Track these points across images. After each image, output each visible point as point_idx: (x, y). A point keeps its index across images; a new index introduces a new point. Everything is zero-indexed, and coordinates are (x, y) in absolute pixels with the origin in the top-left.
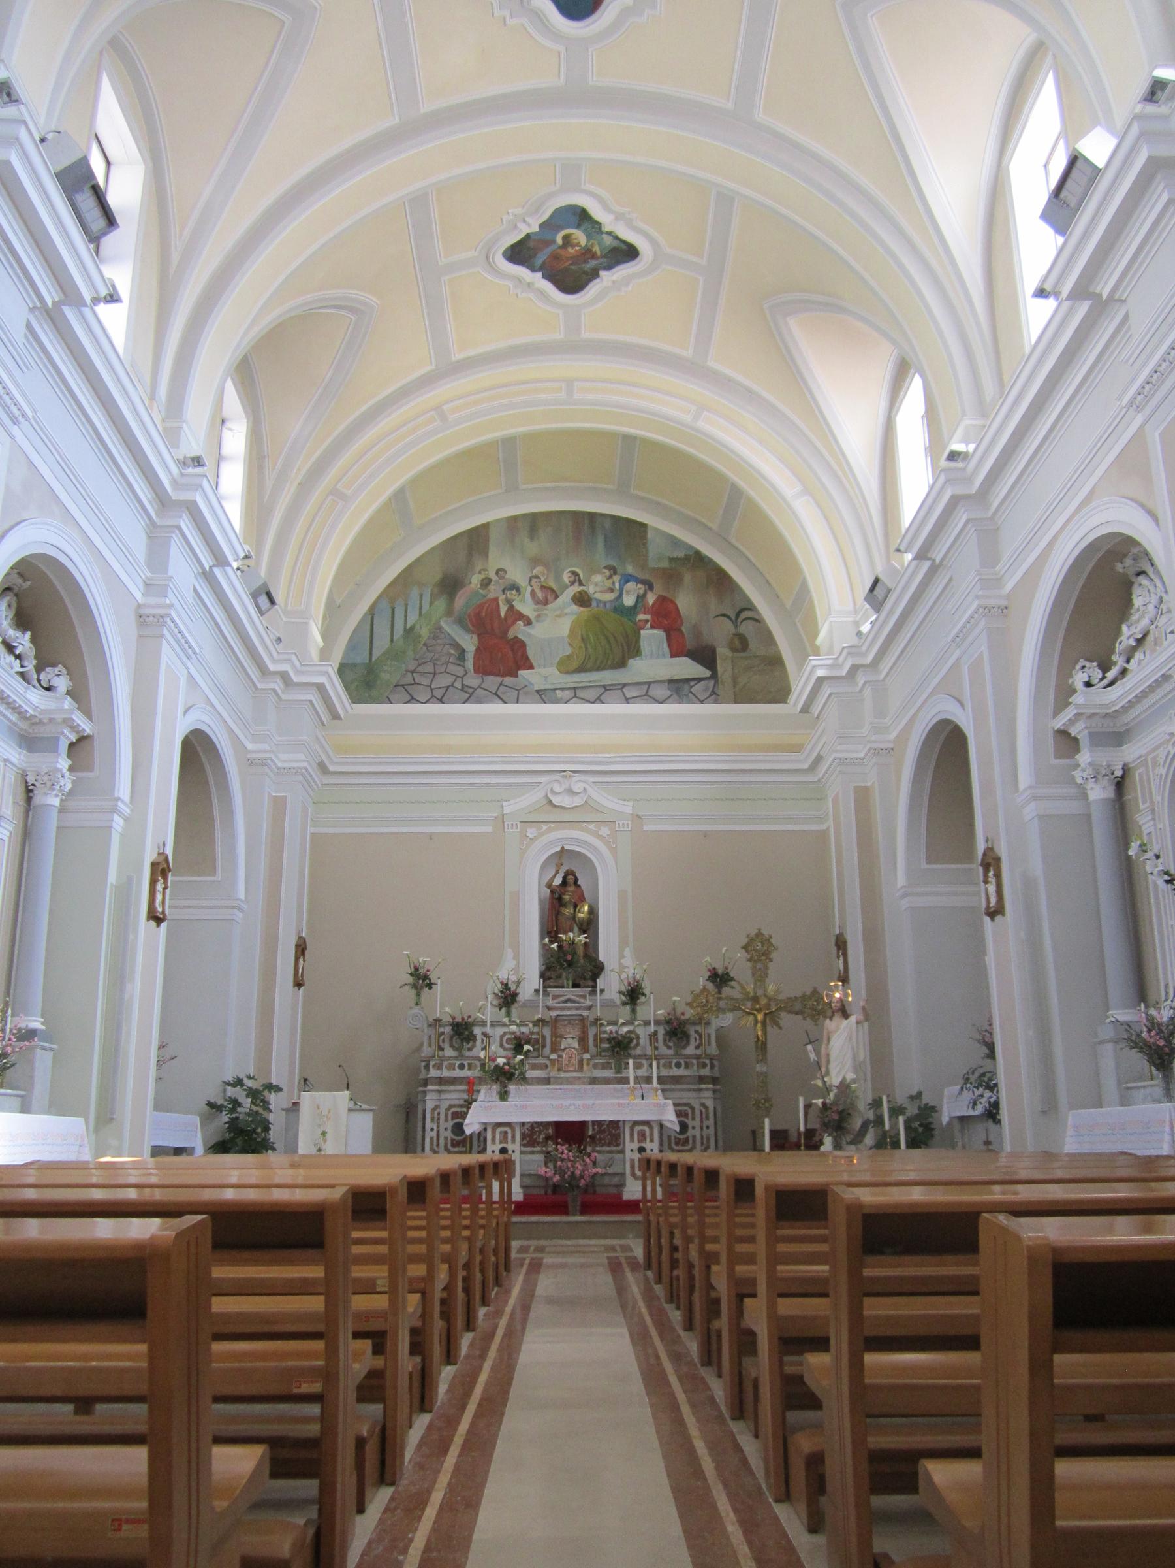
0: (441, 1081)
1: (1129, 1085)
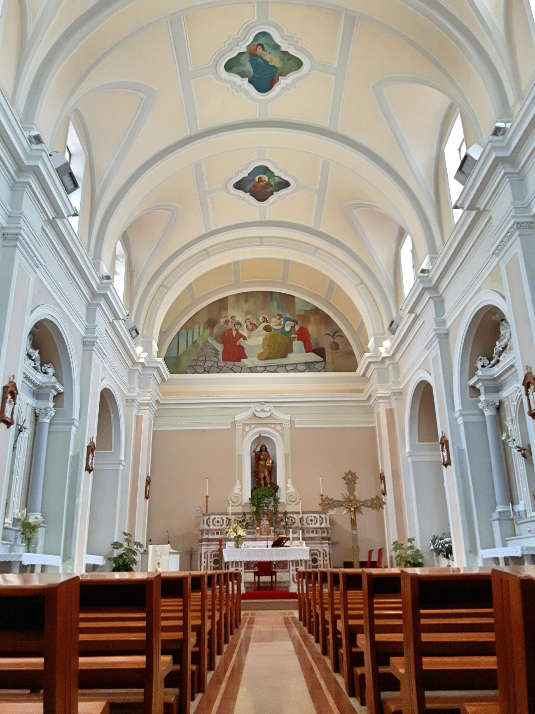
0: (208, 540)
1: (506, 539)
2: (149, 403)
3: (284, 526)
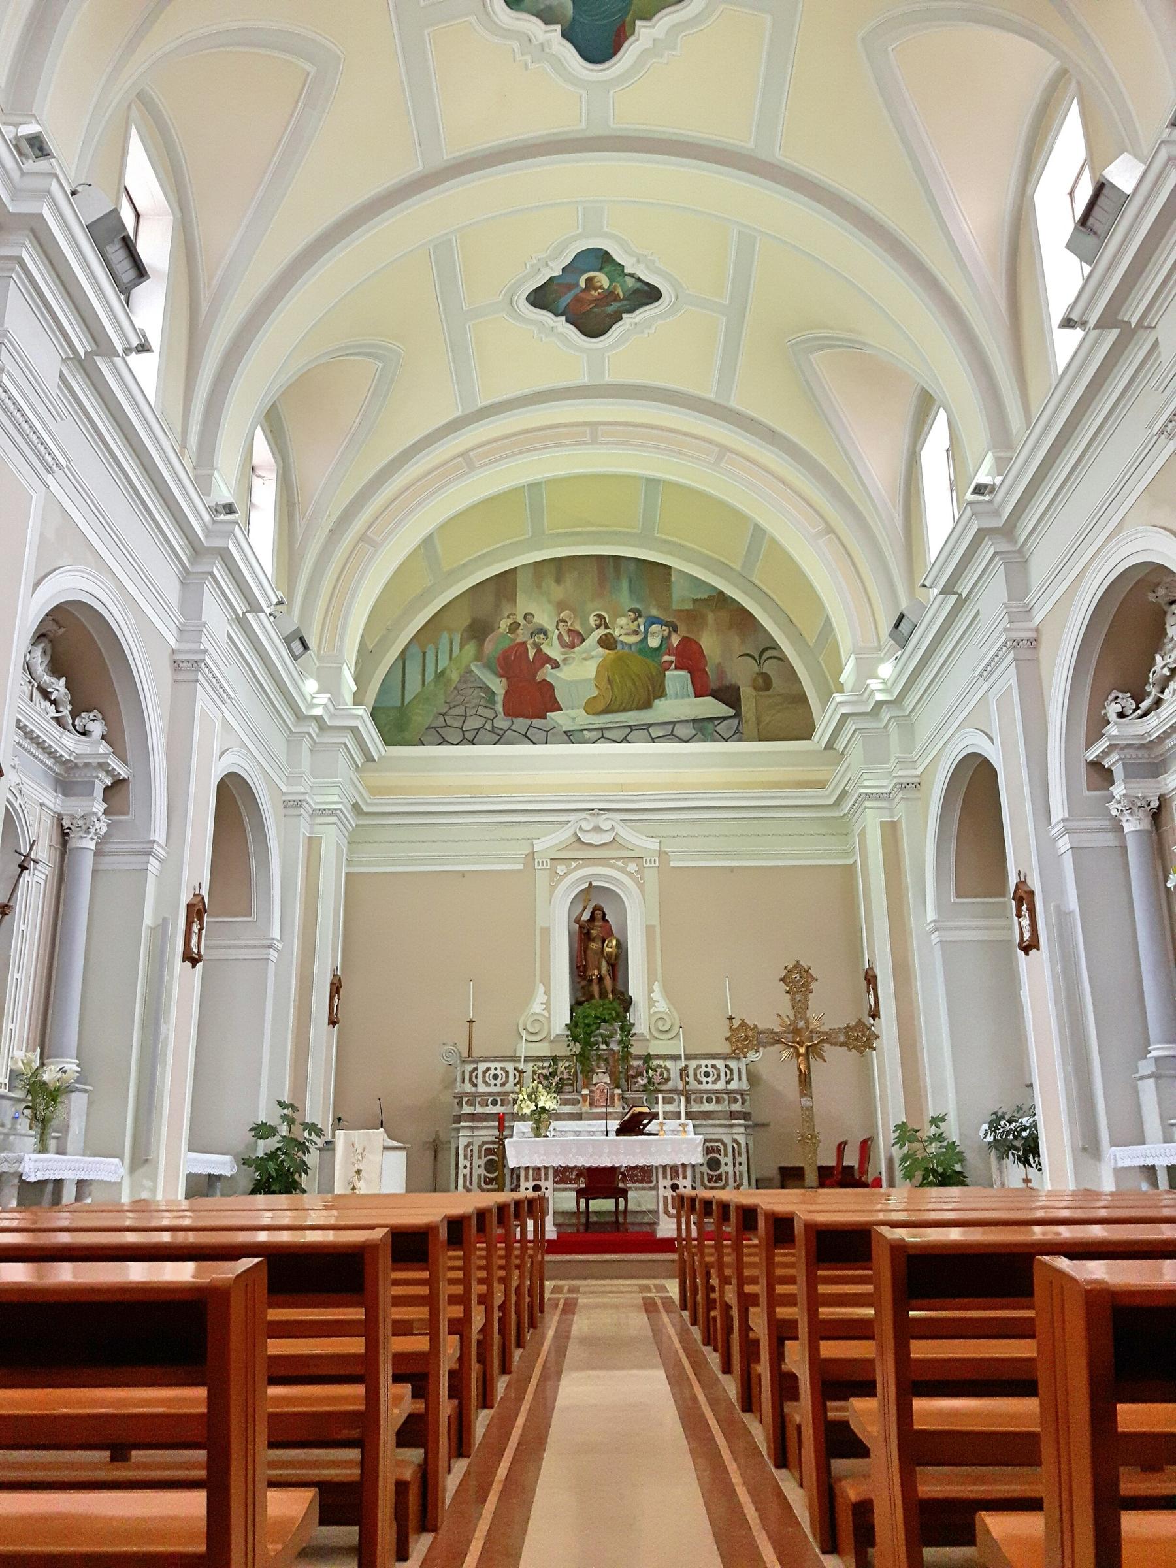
0: (473, 1117)
2: (336, 810)
3: (644, 1085)
